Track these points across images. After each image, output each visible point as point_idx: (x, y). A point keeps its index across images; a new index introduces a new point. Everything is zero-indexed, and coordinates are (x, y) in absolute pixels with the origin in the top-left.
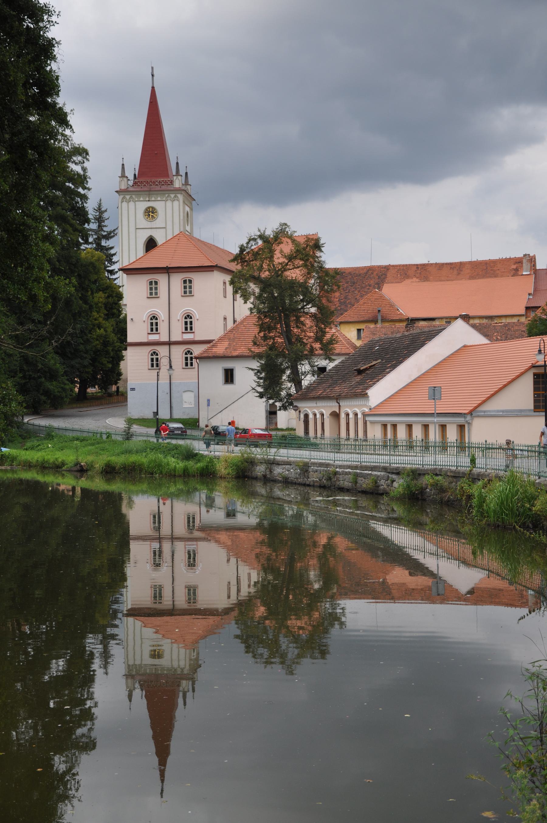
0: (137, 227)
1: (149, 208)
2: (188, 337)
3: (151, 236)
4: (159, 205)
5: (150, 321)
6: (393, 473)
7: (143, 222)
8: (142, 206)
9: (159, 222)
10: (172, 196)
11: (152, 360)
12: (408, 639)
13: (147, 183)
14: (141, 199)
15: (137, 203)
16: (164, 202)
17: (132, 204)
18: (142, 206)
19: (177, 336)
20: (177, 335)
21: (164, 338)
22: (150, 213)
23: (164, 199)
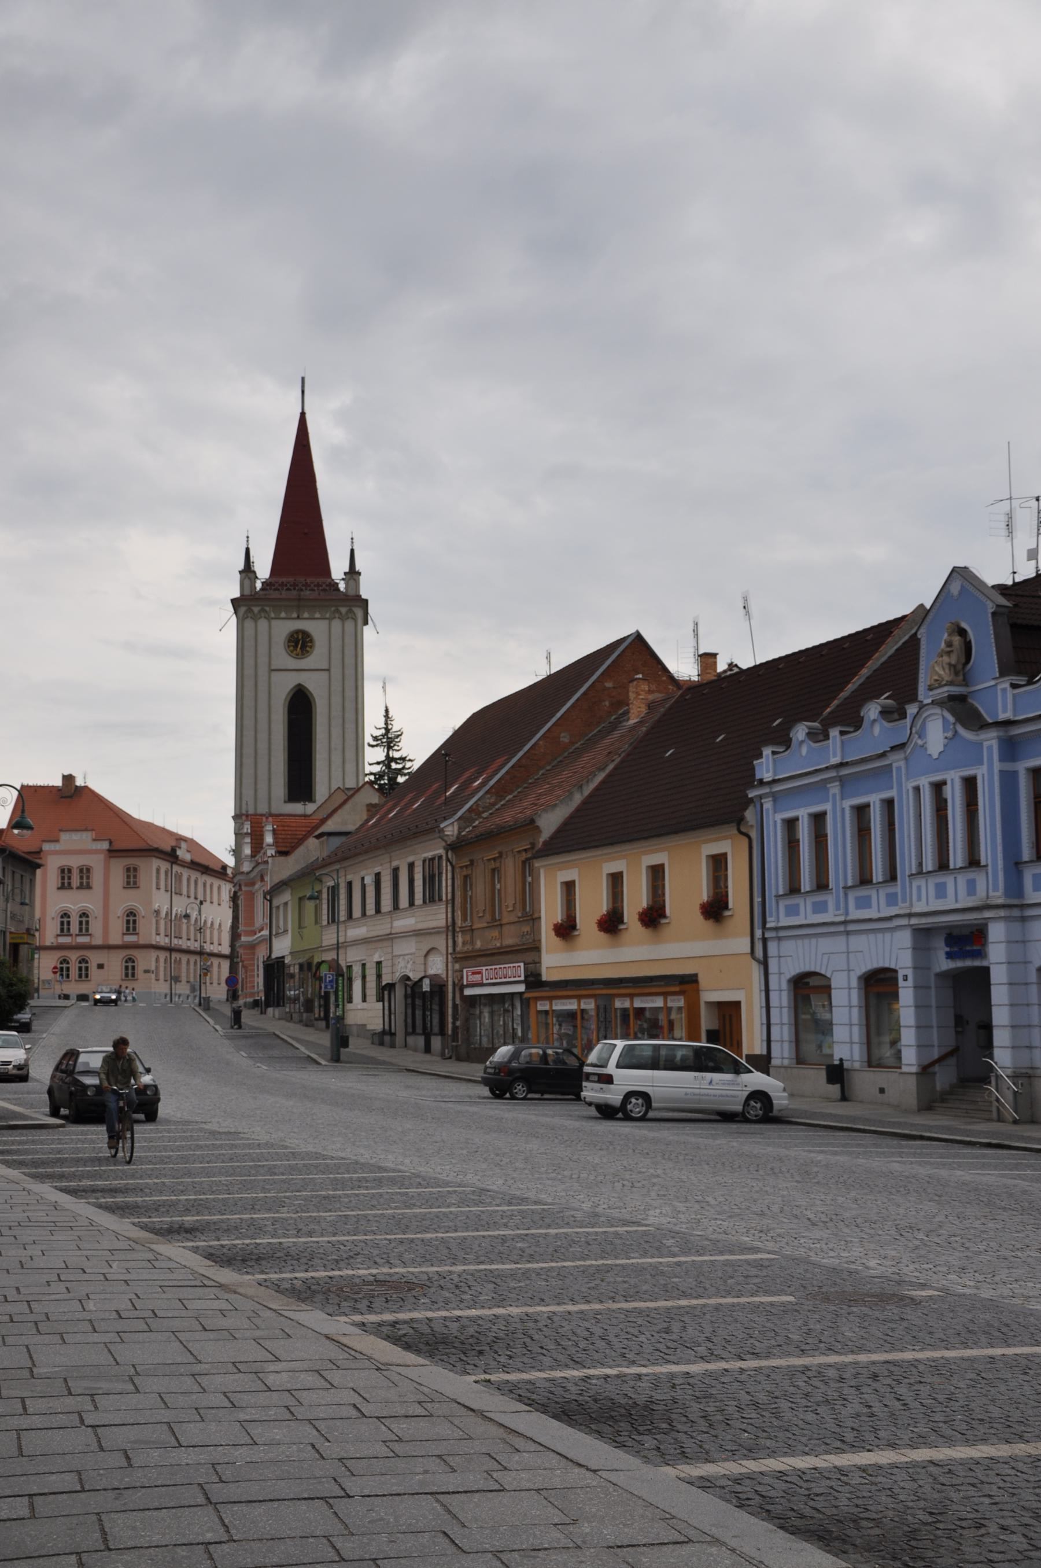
0: (273, 667)
1: (297, 632)
2: (131, 939)
3: (299, 685)
4: (316, 628)
5: (59, 920)
6: (384, 1063)
7: (283, 658)
8: (283, 628)
9: (316, 658)
10: (343, 610)
11: (127, 968)
12: (546, 1096)
13: (306, 585)
14: (283, 615)
15: (274, 623)
16: (327, 622)
17: (263, 624)
18: (283, 628)
19: (115, 939)
20: (116, 937)
21: (98, 941)
22: (300, 643)
23: (328, 616)
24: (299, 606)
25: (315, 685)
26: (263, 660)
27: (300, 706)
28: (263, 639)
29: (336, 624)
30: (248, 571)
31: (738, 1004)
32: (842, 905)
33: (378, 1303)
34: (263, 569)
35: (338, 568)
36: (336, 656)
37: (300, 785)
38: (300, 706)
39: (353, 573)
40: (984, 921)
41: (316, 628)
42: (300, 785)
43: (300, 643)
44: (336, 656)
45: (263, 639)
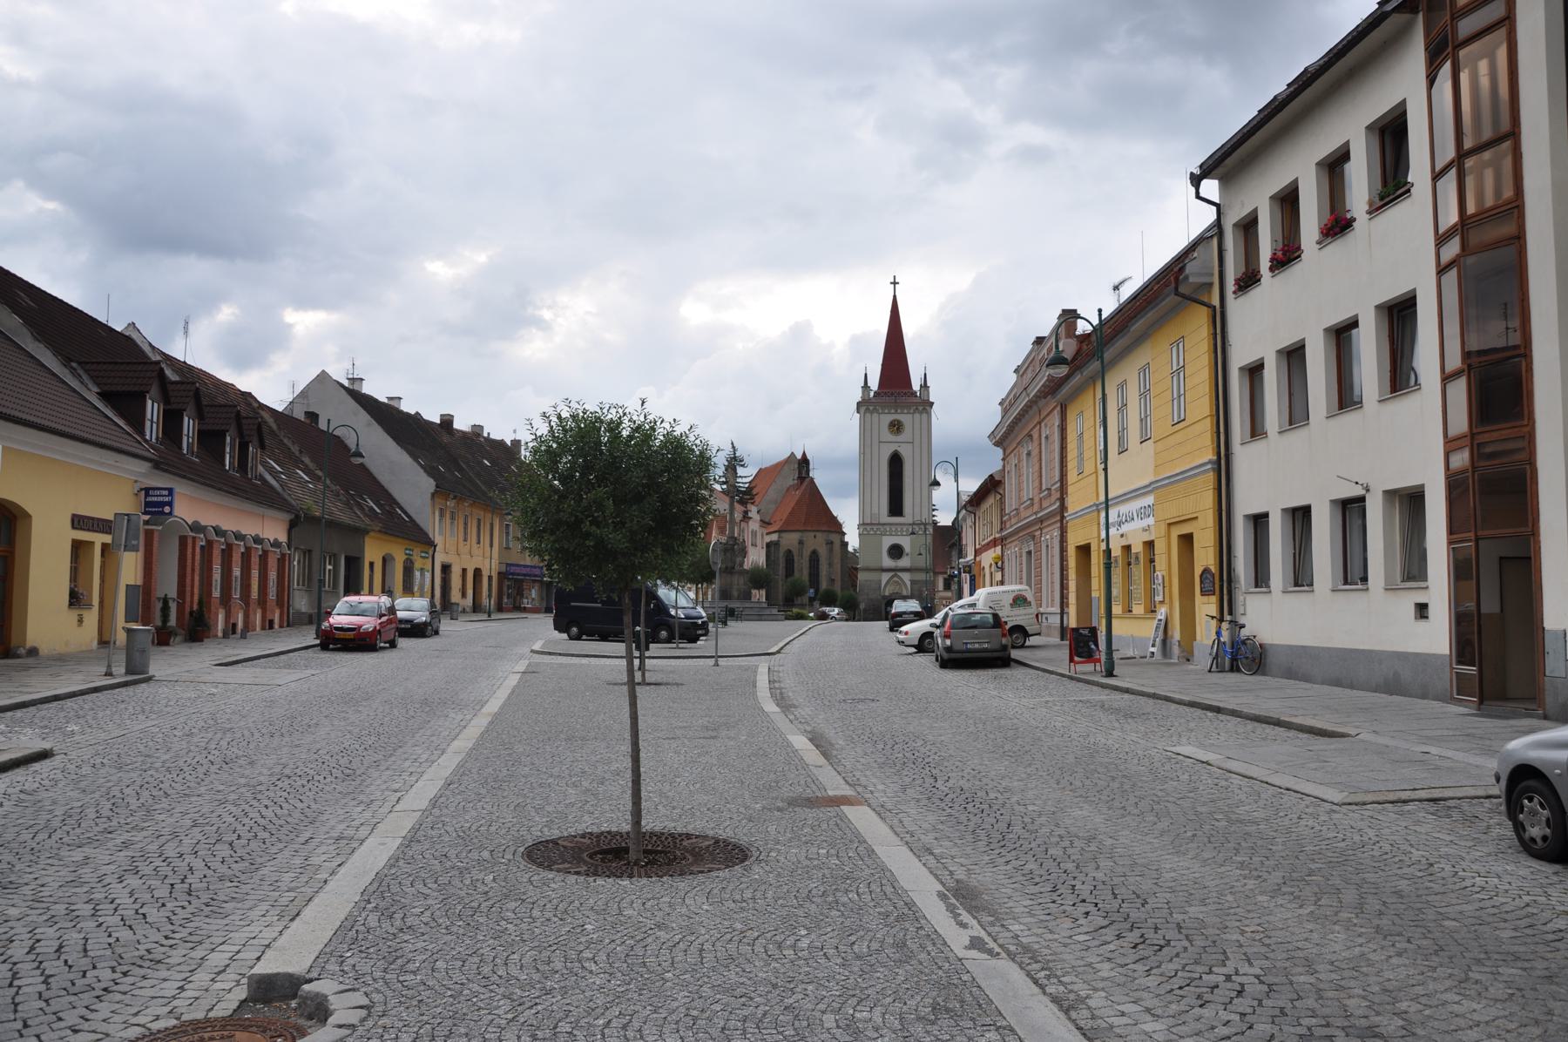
4: (905, 418)
7: (887, 435)
8: (887, 419)
9: (906, 435)
18: (887, 419)
22: (896, 427)
24: (896, 407)
25: (905, 452)
26: (917, 450)
27: (896, 462)
28: (875, 426)
29: (917, 416)
30: (866, 387)
31: (1459, 663)
32: (470, 592)
33: (1184, 740)
34: (874, 384)
35: (916, 386)
36: (917, 432)
37: (896, 507)
38: (896, 462)
39: (925, 386)
40: (1395, 119)
41: (905, 418)
42: (896, 507)
43: (896, 427)
44: (917, 432)
45: (875, 426)
